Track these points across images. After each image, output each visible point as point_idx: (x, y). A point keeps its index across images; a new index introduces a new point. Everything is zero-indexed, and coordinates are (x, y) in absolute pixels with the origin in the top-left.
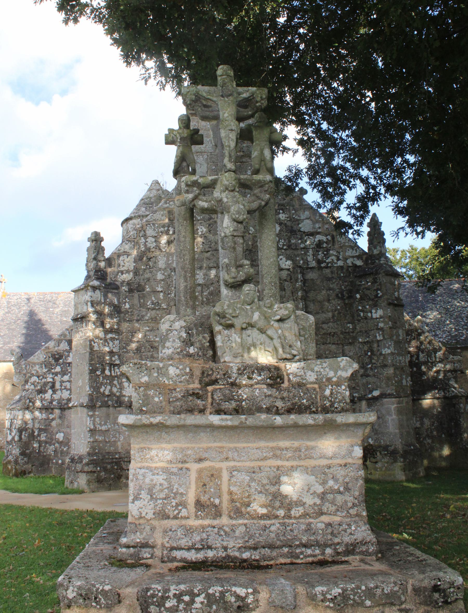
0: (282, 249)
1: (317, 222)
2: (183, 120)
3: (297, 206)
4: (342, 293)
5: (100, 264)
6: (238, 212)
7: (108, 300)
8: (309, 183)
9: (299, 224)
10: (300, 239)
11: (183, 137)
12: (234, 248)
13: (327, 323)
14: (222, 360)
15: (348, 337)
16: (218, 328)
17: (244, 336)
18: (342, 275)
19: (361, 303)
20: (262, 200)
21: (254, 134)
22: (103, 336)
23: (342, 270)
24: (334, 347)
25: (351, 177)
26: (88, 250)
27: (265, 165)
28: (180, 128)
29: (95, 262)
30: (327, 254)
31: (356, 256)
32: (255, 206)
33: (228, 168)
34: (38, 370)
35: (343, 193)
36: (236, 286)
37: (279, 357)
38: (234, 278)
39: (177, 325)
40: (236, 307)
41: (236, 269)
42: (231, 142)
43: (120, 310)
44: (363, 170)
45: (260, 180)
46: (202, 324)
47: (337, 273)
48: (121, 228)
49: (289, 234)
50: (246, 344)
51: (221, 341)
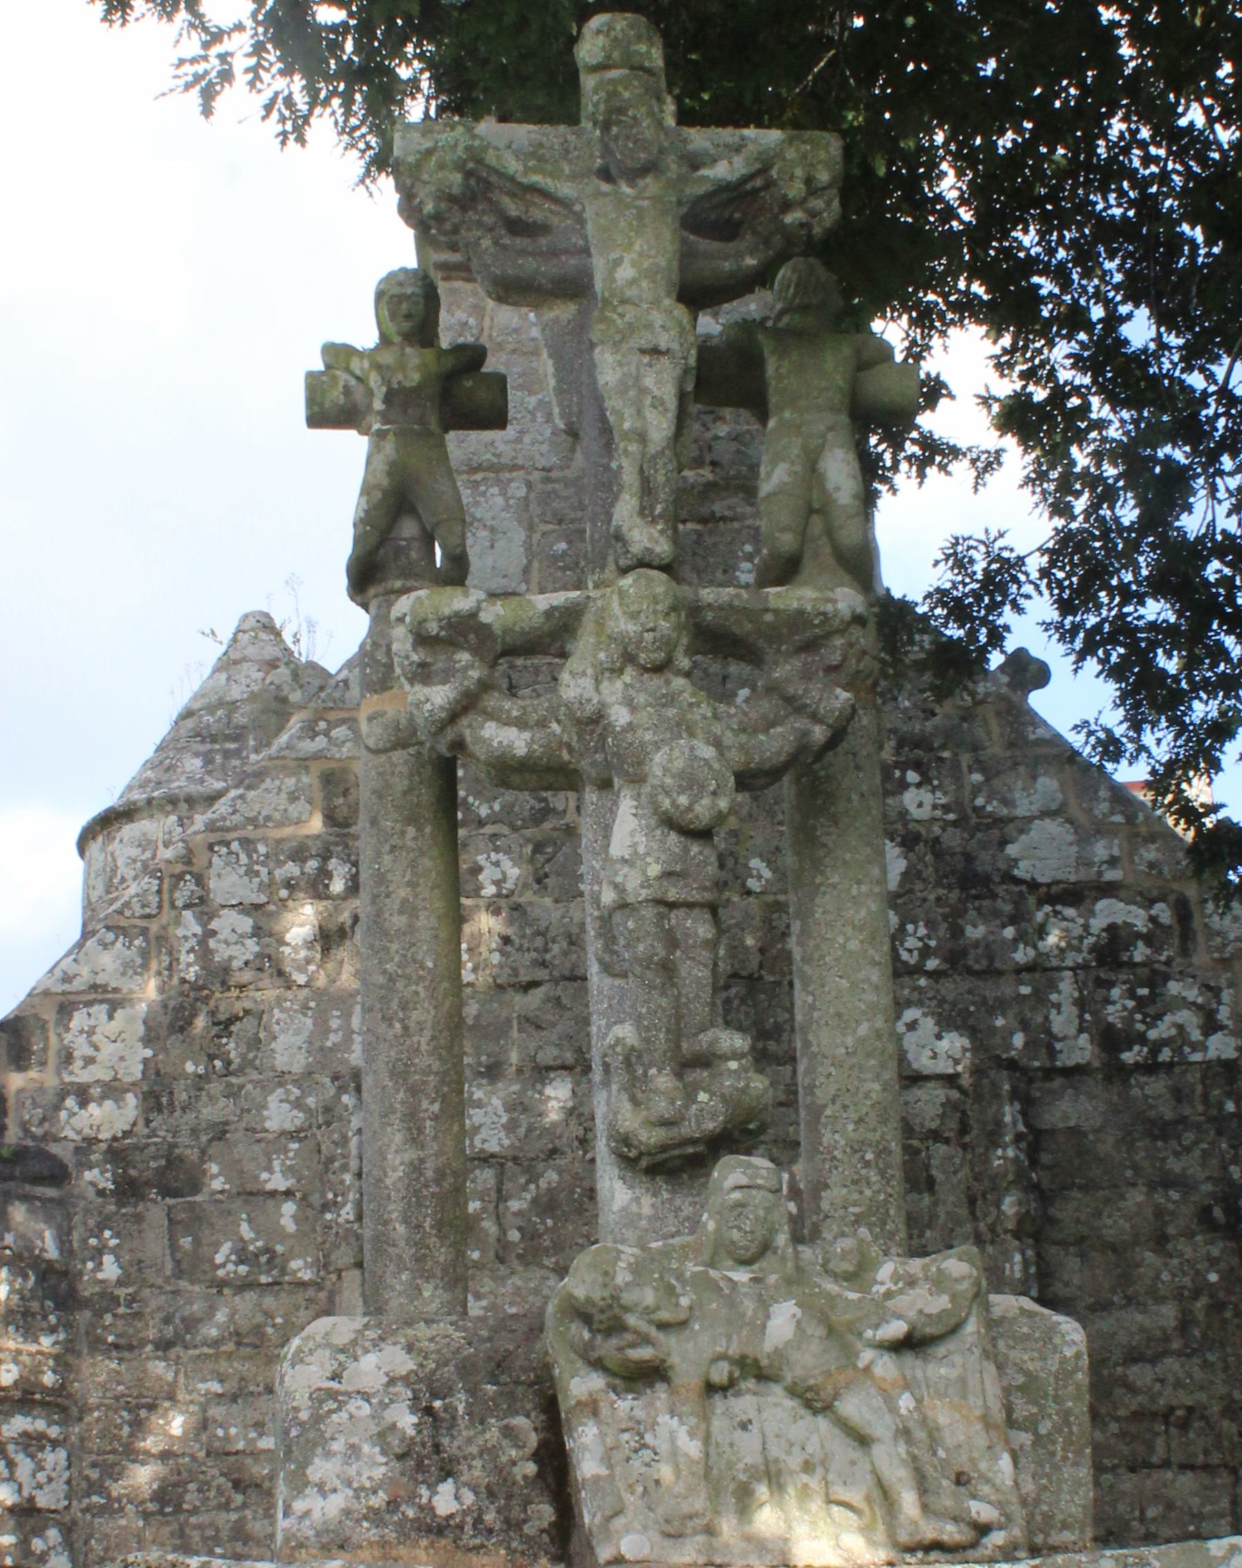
0: (918, 970)
1: (1102, 829)
2: (398, 299)
3: (995, 749)
6: (690, 782)
8: (1059, 626)
9: (1003, 842)
10: (1013, 920)
12: (668, 969)
13: (1153, 1361)
16: (581, 1384)
17: (718, 1425)
18: (1230, 1107)
20: (815, 718)
24: (1186, 1482)
27: (829, 532)
28: (385, 339)
32: (775, 746)
33: (635, 549)
36: (677, 1165)
37: (903, 1537)
38: (666, 1123)
39: (371, 1368)
41: (679, 1075)
42: (651, 416)
43: (72, 1292)
45: (801, 612)
46: (499, 1365)
47: (1205, 1096)
48: (79, 865)
49: (954, 896)
50: (731, 1465)
51: (599, 1451)
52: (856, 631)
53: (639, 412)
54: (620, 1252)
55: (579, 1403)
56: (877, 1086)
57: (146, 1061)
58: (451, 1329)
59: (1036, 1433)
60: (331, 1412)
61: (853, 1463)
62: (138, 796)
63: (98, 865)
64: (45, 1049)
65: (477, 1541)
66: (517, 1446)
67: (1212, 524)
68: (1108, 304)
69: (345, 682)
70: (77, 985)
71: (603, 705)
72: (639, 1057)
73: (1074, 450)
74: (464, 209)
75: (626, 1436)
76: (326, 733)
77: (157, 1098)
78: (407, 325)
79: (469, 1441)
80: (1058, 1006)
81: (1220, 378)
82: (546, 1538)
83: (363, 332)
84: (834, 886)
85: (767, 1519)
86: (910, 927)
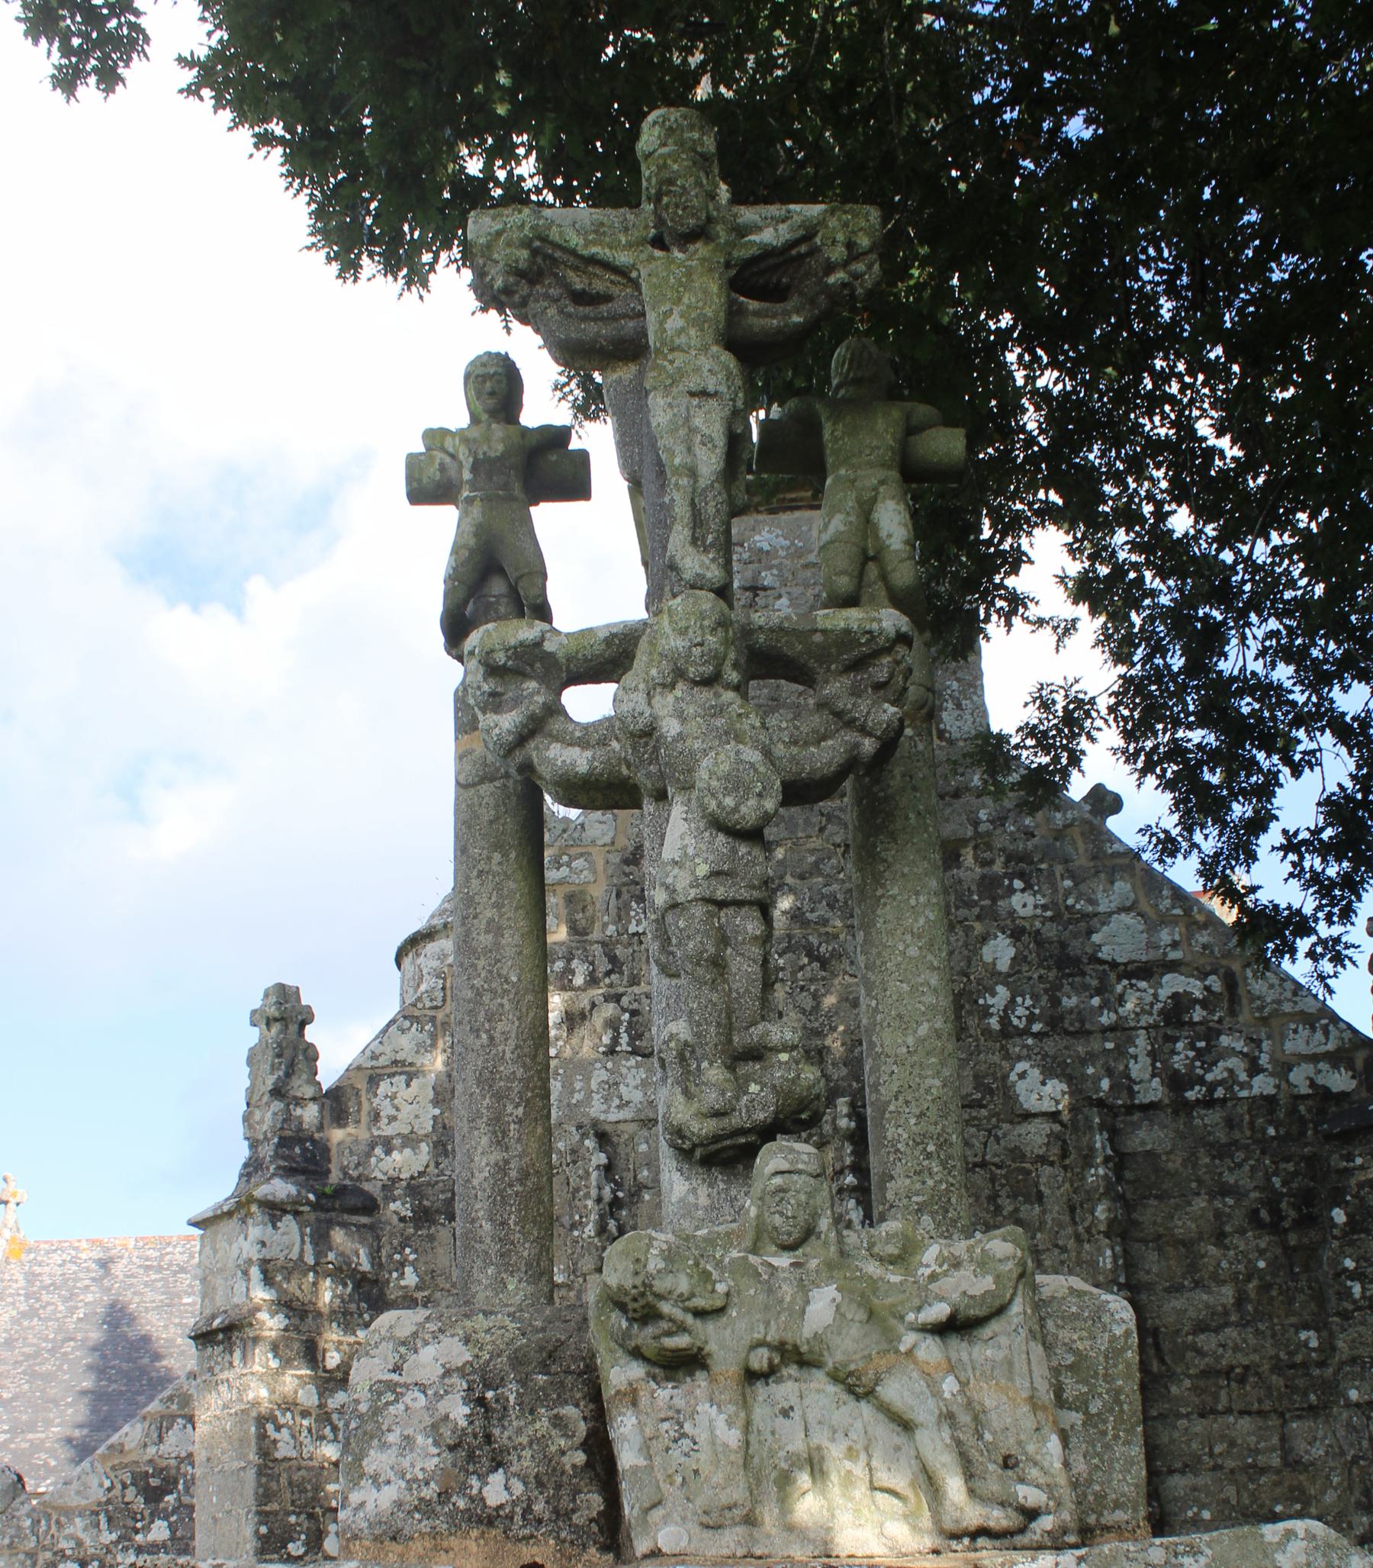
0: (1026, 1032)
1: (1165, 920)
2: (484, 378)
3: (1081, 861)
4: (1272, 1202)
5: (299, 1111)
6: (735, 783)
7: (331, 1256)
8: (1125, 751)
9: (1090, 932)
10: (1098, 992)
11: (487, 460)
12: (718, 964)
13: (1216, 1331)
14: (641, 1547)
15: (1300, 1382)
16: (621, 1374)
17: (761, 1413)
18: (1271, 1131)
19: (1351, 1243)
20: (864, 731)
21: (827, 435)
22: (314, 1400)
23: (1272, 1112)
24: (1245, 1424)
25: (1299, 721)
26: (251, 1061)
27: (884, 577)
28: (475, 419)
29: (278, 1105)
30: (1209, 1048)
31: (1327, 1056)
32: (825, 757)
33: (687, 576)
34: (81, 1535)
35: (1266, 790)
36: (726, 1155)
37: (949, 1525)
38: (718, 1114)
39: (428, 1361)
40: (719, 1264)
41: (731, 1069)
42: (701, 452)
43: (382, 1294)
44: (1345, 689)
45: (847, 631)
46: (550, 1355)
47: (1252, 1123)
48: (398, 974)
49: (1052, 974)
50: (772, 1454)
51: (637, 1440)
52: (901, 650)
53: (689, 449)
54: (651, 1238)
55: (618, 1392)
56: (937, 1083)
57: (435, 1118)
58: (507, 1321)
59: (1086, 1413)
60: (388, 1404)
61: (898, 1449)
62: (438, 922)
63: (409, 975)
64: (359, 1111)
65: (527, 1532)
66: (565, 1435)
67: (1243, 669)
68: (1159, 505)
69: (582, 825)
70: (383, 1061)
71: (655, 718)
72: (693, 1052)
73: (1133, 616)
74: (532, 282)
75: (666, 1425)
76: (568, 865)
77: (444, 1145)
78: (491, 402)
79: (519, 1431)
80: (1135, 1057)
81: (1245, 553)
82: (595, 1528)
83: (456, 416)
84: (894, 897)
85: (808, 1506)
86: (1019, 1000)
